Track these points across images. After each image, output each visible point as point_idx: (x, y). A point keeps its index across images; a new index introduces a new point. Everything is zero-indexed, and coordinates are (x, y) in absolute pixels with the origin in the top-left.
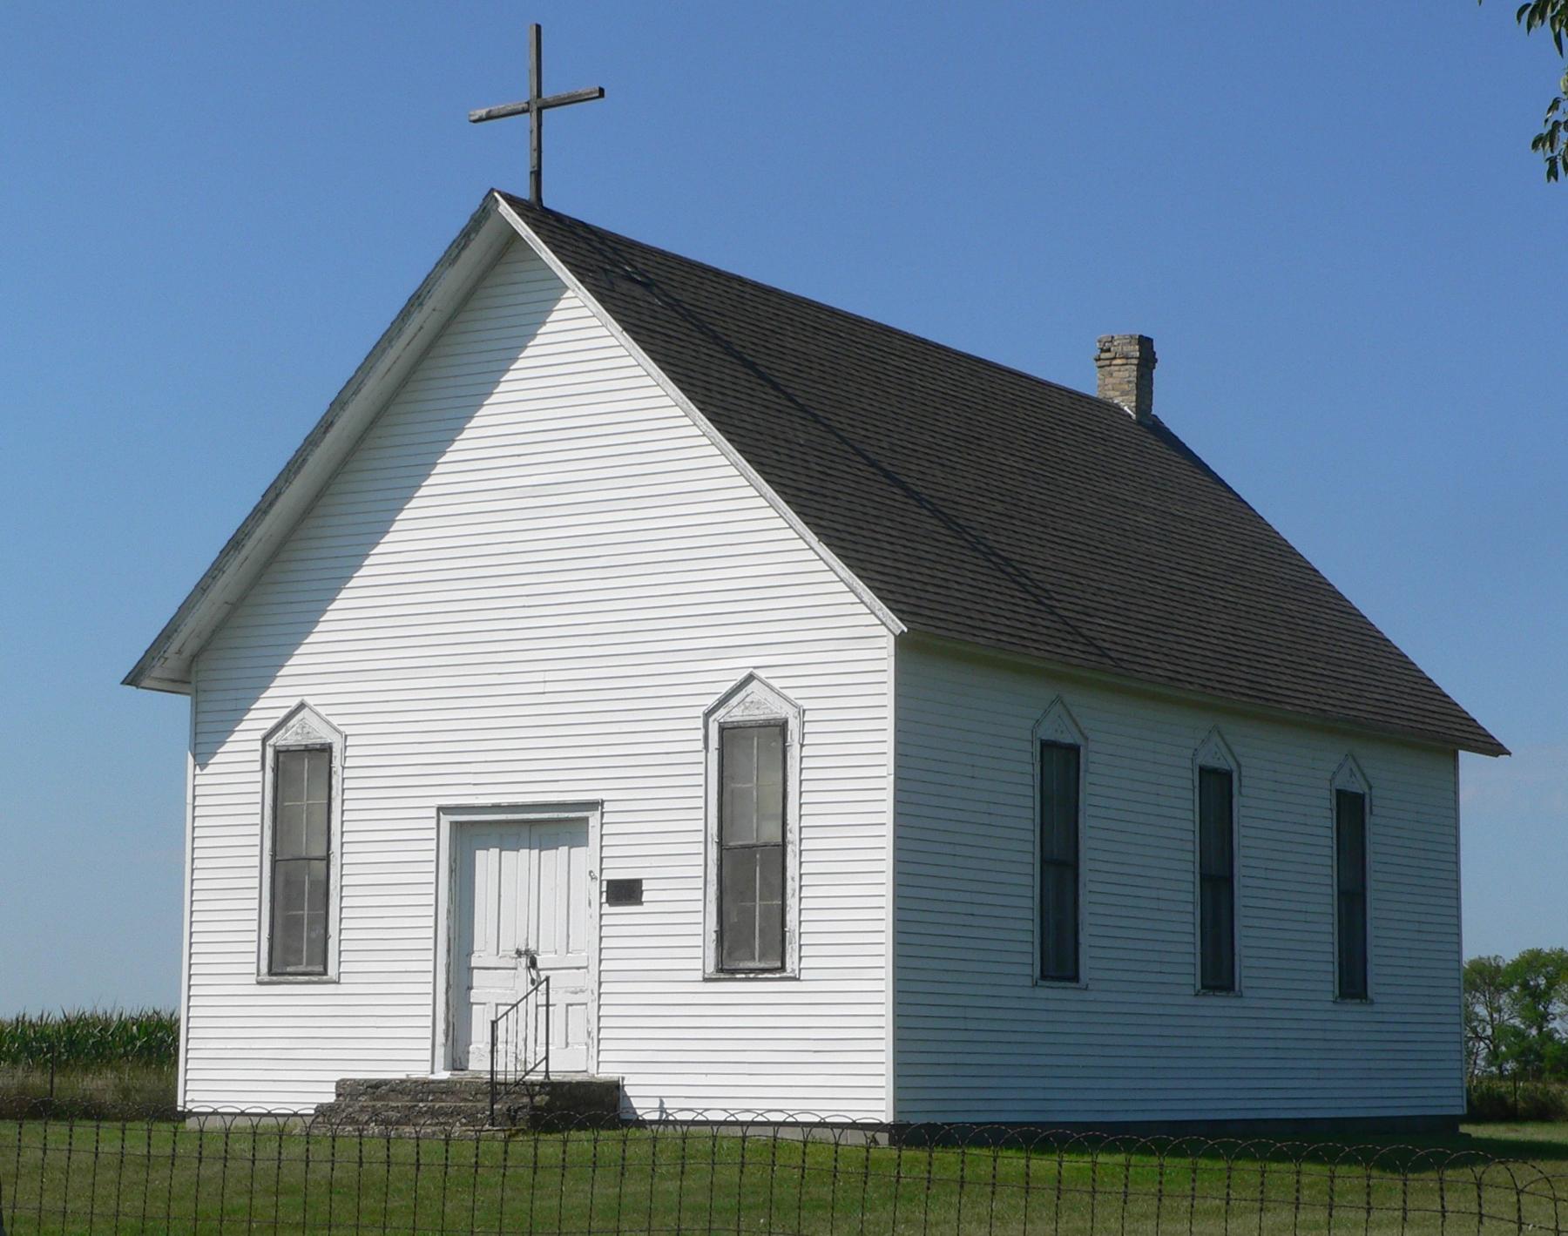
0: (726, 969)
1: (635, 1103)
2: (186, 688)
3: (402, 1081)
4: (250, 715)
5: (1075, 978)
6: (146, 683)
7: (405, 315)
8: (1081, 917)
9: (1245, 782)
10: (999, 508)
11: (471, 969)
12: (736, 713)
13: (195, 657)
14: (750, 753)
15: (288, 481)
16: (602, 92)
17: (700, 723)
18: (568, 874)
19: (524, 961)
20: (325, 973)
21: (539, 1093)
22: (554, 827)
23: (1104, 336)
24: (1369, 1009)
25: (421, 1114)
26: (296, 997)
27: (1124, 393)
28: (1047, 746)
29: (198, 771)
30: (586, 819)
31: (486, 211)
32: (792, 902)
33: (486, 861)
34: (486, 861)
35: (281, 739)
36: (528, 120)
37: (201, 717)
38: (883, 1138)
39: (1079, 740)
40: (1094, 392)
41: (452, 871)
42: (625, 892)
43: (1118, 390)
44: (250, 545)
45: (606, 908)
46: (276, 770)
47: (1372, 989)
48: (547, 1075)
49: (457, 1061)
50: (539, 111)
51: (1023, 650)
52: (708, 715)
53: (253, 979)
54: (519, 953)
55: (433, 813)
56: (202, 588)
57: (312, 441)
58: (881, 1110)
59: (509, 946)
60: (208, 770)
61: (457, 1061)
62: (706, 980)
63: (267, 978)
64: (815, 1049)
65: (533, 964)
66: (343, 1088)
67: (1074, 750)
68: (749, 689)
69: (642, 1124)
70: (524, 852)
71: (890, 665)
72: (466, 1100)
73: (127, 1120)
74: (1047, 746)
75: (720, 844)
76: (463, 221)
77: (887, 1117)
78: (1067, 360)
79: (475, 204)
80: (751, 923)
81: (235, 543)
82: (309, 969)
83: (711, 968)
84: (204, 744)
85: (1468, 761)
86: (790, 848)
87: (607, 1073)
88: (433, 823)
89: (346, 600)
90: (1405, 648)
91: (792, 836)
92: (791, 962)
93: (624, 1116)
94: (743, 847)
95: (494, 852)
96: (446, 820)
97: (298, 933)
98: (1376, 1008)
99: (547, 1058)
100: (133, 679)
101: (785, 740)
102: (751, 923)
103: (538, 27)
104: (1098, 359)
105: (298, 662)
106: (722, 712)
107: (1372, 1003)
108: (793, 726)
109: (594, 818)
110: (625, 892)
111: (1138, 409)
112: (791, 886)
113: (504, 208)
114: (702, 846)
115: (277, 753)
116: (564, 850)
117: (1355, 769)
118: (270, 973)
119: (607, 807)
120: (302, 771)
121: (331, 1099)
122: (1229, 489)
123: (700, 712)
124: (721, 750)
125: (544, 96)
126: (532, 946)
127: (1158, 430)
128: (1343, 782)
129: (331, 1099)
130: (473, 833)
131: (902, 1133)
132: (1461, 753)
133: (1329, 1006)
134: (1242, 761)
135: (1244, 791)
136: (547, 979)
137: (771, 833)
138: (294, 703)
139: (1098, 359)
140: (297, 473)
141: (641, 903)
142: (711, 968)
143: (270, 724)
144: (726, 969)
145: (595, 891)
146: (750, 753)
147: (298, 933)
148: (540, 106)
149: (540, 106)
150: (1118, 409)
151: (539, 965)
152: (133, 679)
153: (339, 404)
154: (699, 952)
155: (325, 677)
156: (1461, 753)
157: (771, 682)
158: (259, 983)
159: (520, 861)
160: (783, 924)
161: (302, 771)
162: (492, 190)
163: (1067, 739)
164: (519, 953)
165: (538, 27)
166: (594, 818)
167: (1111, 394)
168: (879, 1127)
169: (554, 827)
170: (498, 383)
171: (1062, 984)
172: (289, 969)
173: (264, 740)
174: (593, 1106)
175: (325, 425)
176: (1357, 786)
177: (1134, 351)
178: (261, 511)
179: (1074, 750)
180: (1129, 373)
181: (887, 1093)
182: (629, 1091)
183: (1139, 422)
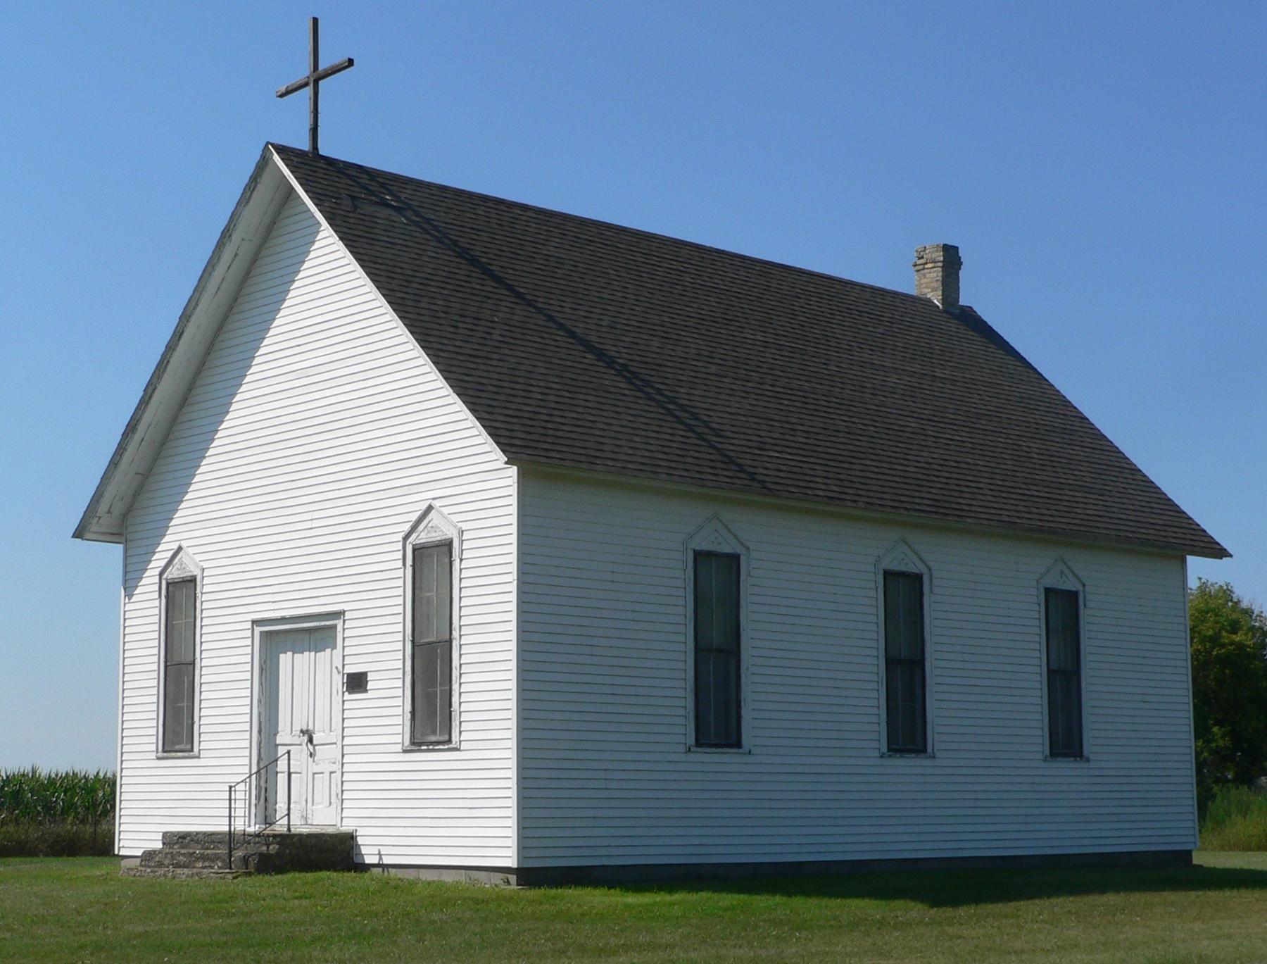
0: (417, 743)
1: (364, 850)
2: (123, 539)
5: (738, 745)
6: (88, 536)
7: (220, 245)
8: (743, 696)
9: (935, 582)
10: (713, 369)
11: (277, 745)
12: (422, 537)
13: (125, 516)
14: (431, 564)
15: (159, 378)
16: (351, 62)
17: (400, 546)
19: (306, 738)
20: (192, 750)
21: (273, 843)
23: (920, 247)
24: (1086, 765)
27: (934, 290)
28: (701, 558)
30: (335, 627)
31: (265, 161)
32: (455, 687)
33: (285, 659)
34: (285, 659)
36: (308, 91)
37: (130, 560)
39: (738, 549)
40: (914, 292)
41: (261, 669)
42: (357, 683)
43: (929, 288)
44: (141, 429)
46: (167, 597)
47: (1087, 749)
48: (289, 829)
49: (268, 820)
50: (316, 82)
51: (560, 462)
53: (153, 756)
54: (302, 731)
55: (249, 625)
56: (114, 463)
57: (171, 347)
58: (509, 858)
59: (297, 728)
62: (405, 751)
63: (160, 754)
64: (448, 811)
65: (311, 740)
66: (169, 839)
67: (735, 558)
69: (366, 868)
70: (306, 654)
71: (514, 491)
73: (378, 865)
74: (701, 558)
75: (413, 641)
76: (250, 169)
77: (512, 862)
78: (895, 269)
79: (257, 156)
81: (131, 428)
83: (407, 742)
84: (130, 583)
87: (347, 826)
88: (249, 633)
90: (1152, 476)
91: (455, 634)
93: (357, 860)
94: (429, 644)
96: (258, 630)
98: (1092, 764)
99: (288, 815)
100: (79, 534)
101: (451, 556)
103: (315, 21)
104: (915, 265)
106: (414, 536)
107: (1088, 760)
108: (456, 544)
110: (357, 683)
111: (944, 301)
112: (455, 673)
113: (276, 157)
114: (401, 644)
115: (168, 584)
117: (1067, 571)
118: (164, 751)
119: (348, 616)
120: (181, 595)
121: (159, 845)
122: (1023, 360)
123: (400, 537)
124: (413, 566)
125: (321, 68)
126: (311, 727)
127: (970, 319)
128: (1053, 581)
129: (159, 845)
131: (528, 875)
132: (1190, 558)
133: (1042, 764)
134: (931, 564)
135: (936, 590)
136: (289, 752)
139: (915, 265)
140: (164, 370)
141: (366, 691)
142: (691, 740)
144: (417, 743)
145: (338, 681)
146: (431, 564)
148: (318, 77)
149: (318, 77)
150: (930, 301)
152: (79, 534)
153: (185, 317)
154: (399, 729)
155: (206, 526)
156: (1190, 558)
158: (158, 758)
160: (450, 706)
162: (268, 143)
163: (727, 549)
164: (302, 731)
165: (315, 21)
167: (926, 290)
169: (315, 632)
171: (714, 750)
172: (177, 747)
174: (336, 852)
175: (178, 334)
176: (1069, 585)
177: (939, 256)
178: (144, 403)
179: (735, 558)
180: (935, 274)
181: (513, 842)
182: (360, 841)
183: (945, 311)
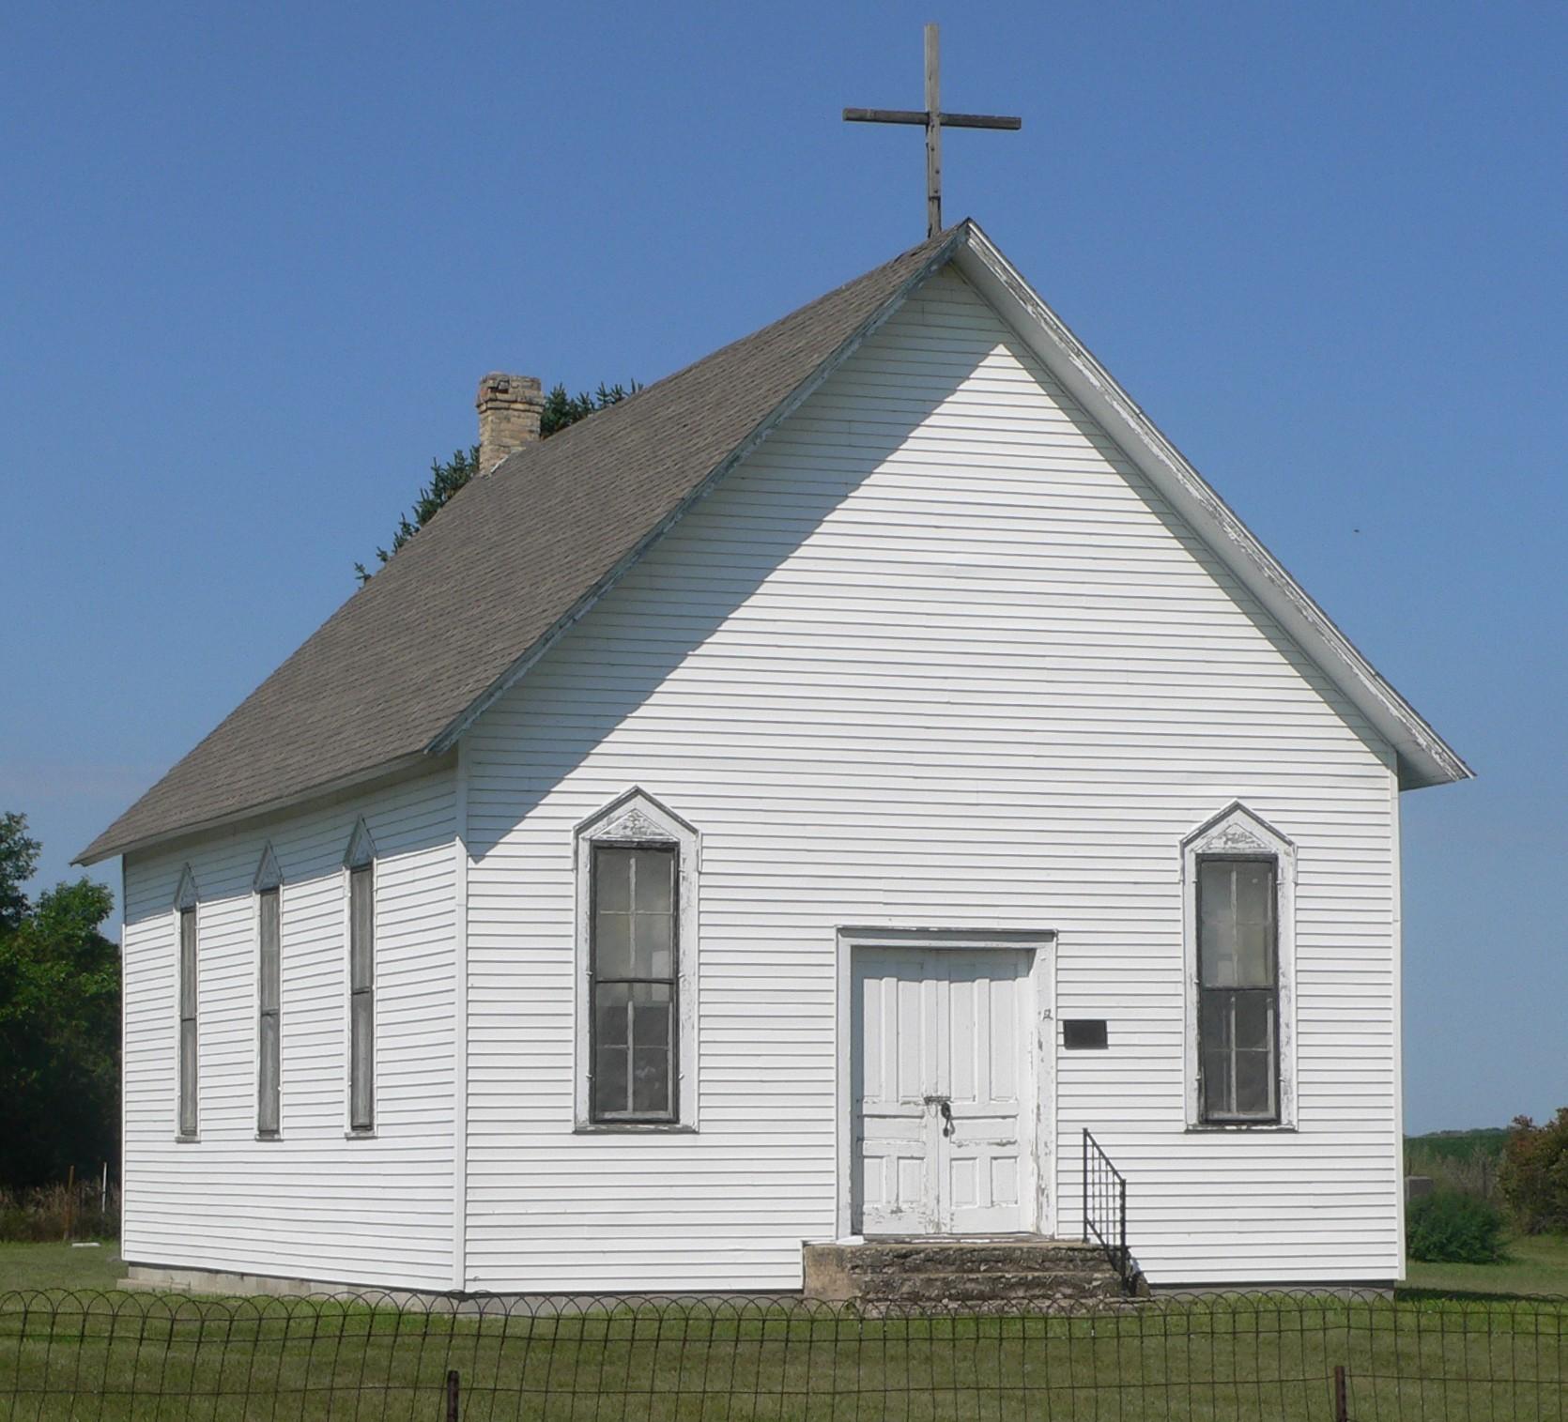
0: (1209, 1122)
3: (1030, 1250)
4: (549, 799)
12: (612, 830)
14: (1237, 884)
18: (1027, 1004)
22: (993, 955)
25: (1012, 1287)
29: (471, 864)
30: (1033, 951)
33: (880, 991)
34: (869, 984)
35: (598, 832)
38: (1390, 1295)
42: (1085, 1034)
45: (1064, 1052)
52: (1185, 844)
54: (928, 1100)
60: (482, 864)
65: (946, 1110)
68: (1231, 819)
72: (1031, 1269)
75: (1199, 985)
80: (1238, 1064)
82: (639, 1115)
86: (1282, 993)
89: (691, 669)
92: (686, 1118)
95: (888, 983)
101: (1275, 878)
102: (1238, 1064)
103: (1012, 124)
105: (617, 741)
108: (1283, 862)
109: (1044, 951)
110: (1085, 1034)
116: (981, 984)
119: (1062, 938)
120: (634, 873)
123: (1176, 840)
130: (881, 955)
137: (1259, 978)
138: (624, 789)
142: (1194, 1120)
143: (587, 813)
144: (1209, 1122)
145: (1054, 1035)
146: (1237, 884)
151: (953, 1113)
157: (1259, 814)
159: (928, 992)
161: (634, 873)
165: (1012, 124)
168: (1387, 1284)
169: (993, 955)
170: (905, 438)
172: (608, 1116)
173: (579, 831)
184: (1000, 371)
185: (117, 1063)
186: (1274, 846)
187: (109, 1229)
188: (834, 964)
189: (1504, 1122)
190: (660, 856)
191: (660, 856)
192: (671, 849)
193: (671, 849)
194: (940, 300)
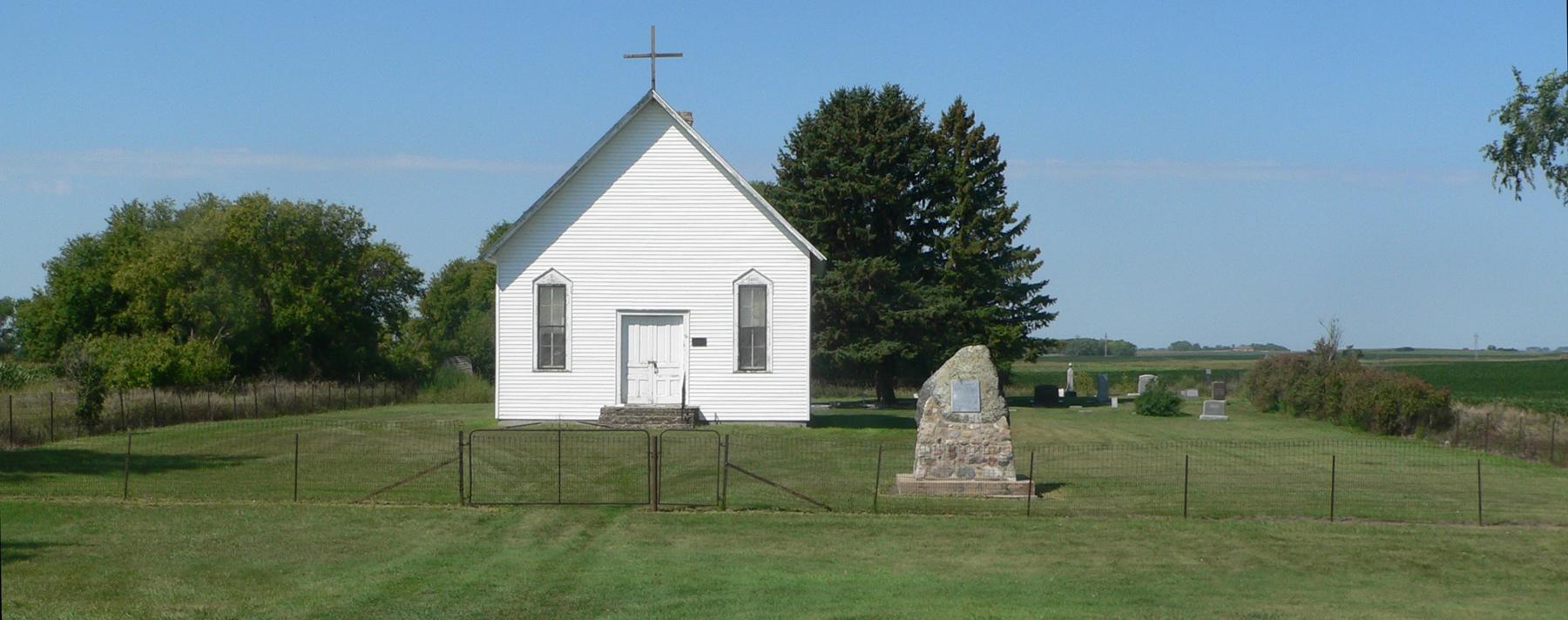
12: (745, 281)
14: (752, 295)
18: (679, 335)
26: (551, 378)
33: (633, 330)
35: (540, 281)
42: (699, 342)
61: (624, 401)
64: (783, 393)
69: (706, 423)
80: (752, 349)
85: (772, 178)
89: (570, 231)
92: (769, 367)
97: (551, 350)
102: (752, 349)
109: (686, 316)
110: (699, 342)
120: (551, 295)
130: (629, 318)
145: (688, 342)
146: (752, 295)
147: (551, 350)
159: (649, 330)
161: (551, 295)
166: (686, 316)
184: (673, 132)
185: (814, 344)
186: (765, 282)
187: (488, 399)
188: (615, 323)
189: (1301, 341)
190: (762, 290)
191: (762, 290)
192: (564, 286)
193: (564, 286)
194: (643, 120)
